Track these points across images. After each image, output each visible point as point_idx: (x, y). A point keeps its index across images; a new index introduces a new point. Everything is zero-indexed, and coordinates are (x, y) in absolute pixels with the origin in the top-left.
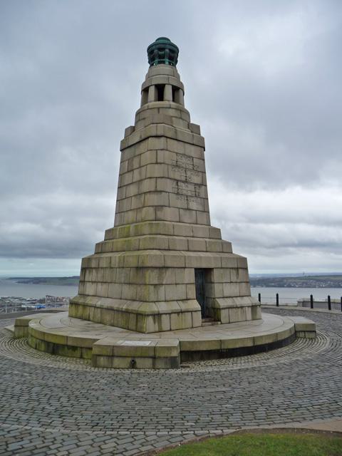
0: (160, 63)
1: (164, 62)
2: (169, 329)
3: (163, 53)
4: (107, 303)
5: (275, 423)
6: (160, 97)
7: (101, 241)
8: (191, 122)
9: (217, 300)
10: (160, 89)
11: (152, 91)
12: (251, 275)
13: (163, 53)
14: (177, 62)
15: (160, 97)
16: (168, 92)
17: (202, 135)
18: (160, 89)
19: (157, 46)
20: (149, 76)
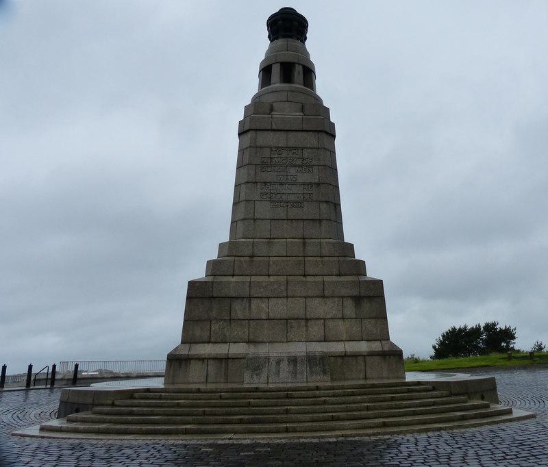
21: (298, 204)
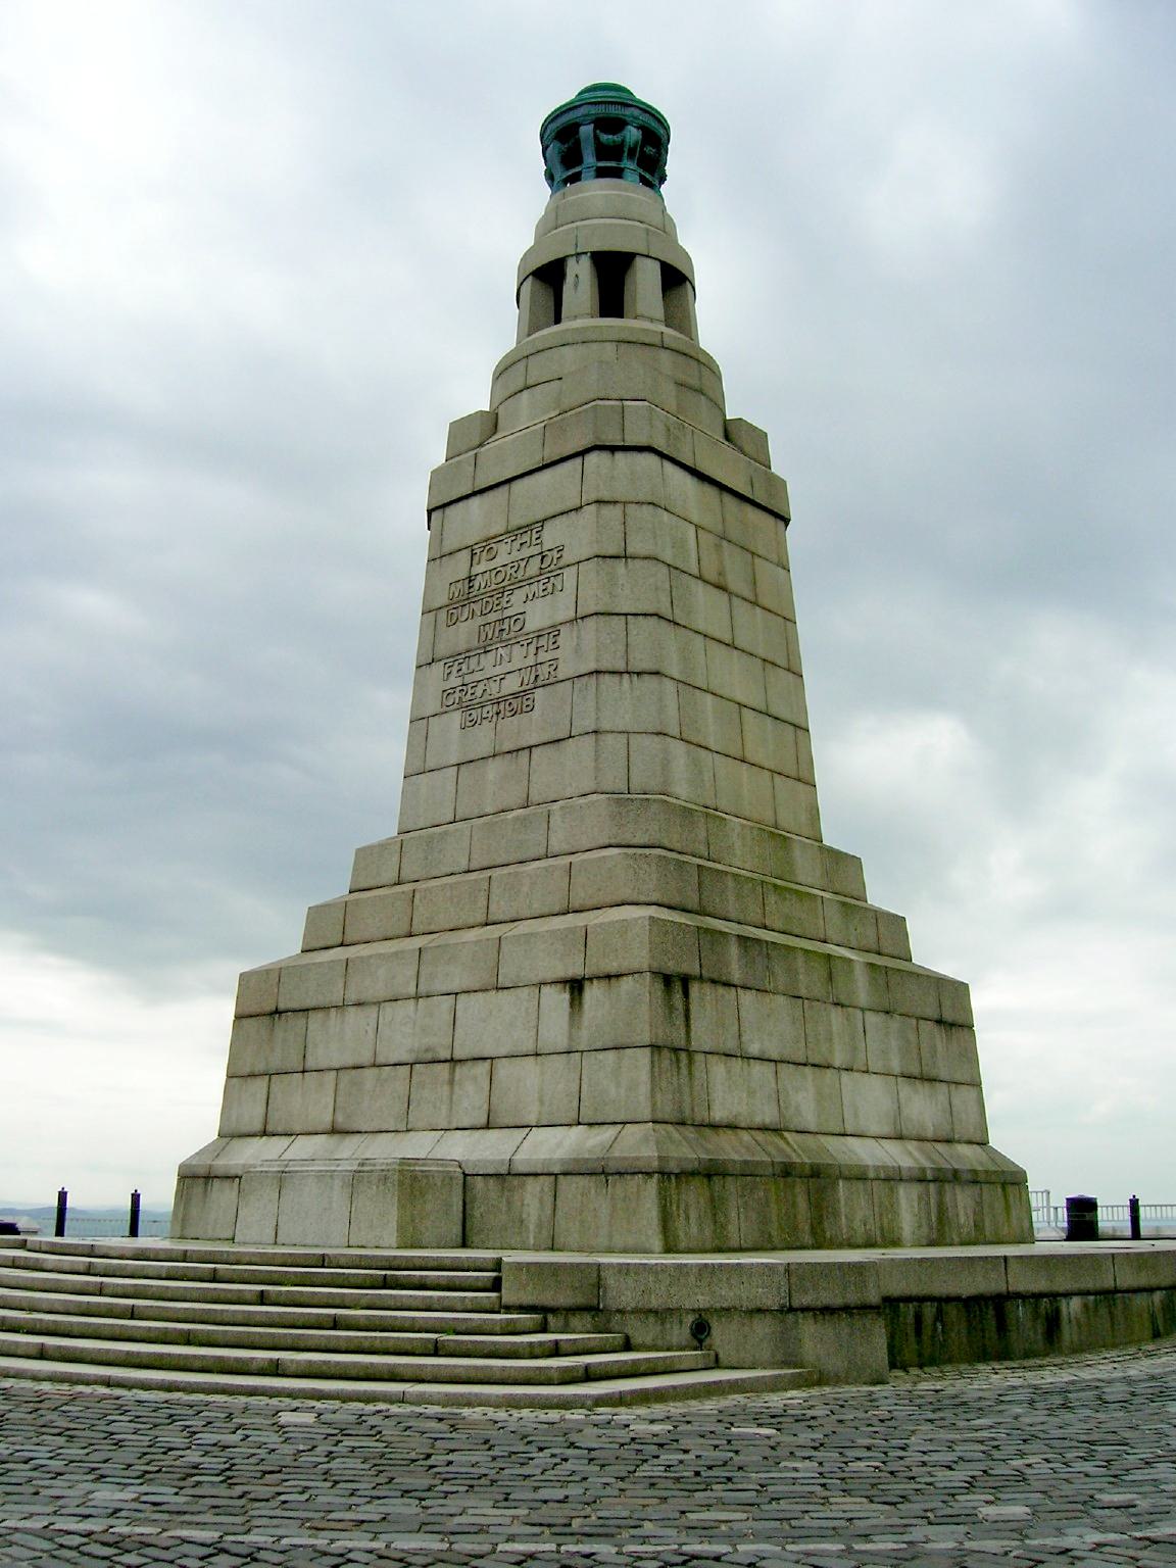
0: (601, 173)
1: (617, 173)
2: (258, 1126)
3: (617, 138)
4: (275, 1169)
5: (824, 1478)
6: (612, 301)
7: (440, 464)
8: (728, 418)
9: (517, 1157)
10: (612, 270)
11: (581, 284)
12: (72, 1209)
13: (617, 138)
14: (663, 179)
15: (612, 301)
16: (645, 281)
17: (776, 468)
18: (612, 270)
19: (593, 110)
20: (549, 226)
21: (518, 702)
